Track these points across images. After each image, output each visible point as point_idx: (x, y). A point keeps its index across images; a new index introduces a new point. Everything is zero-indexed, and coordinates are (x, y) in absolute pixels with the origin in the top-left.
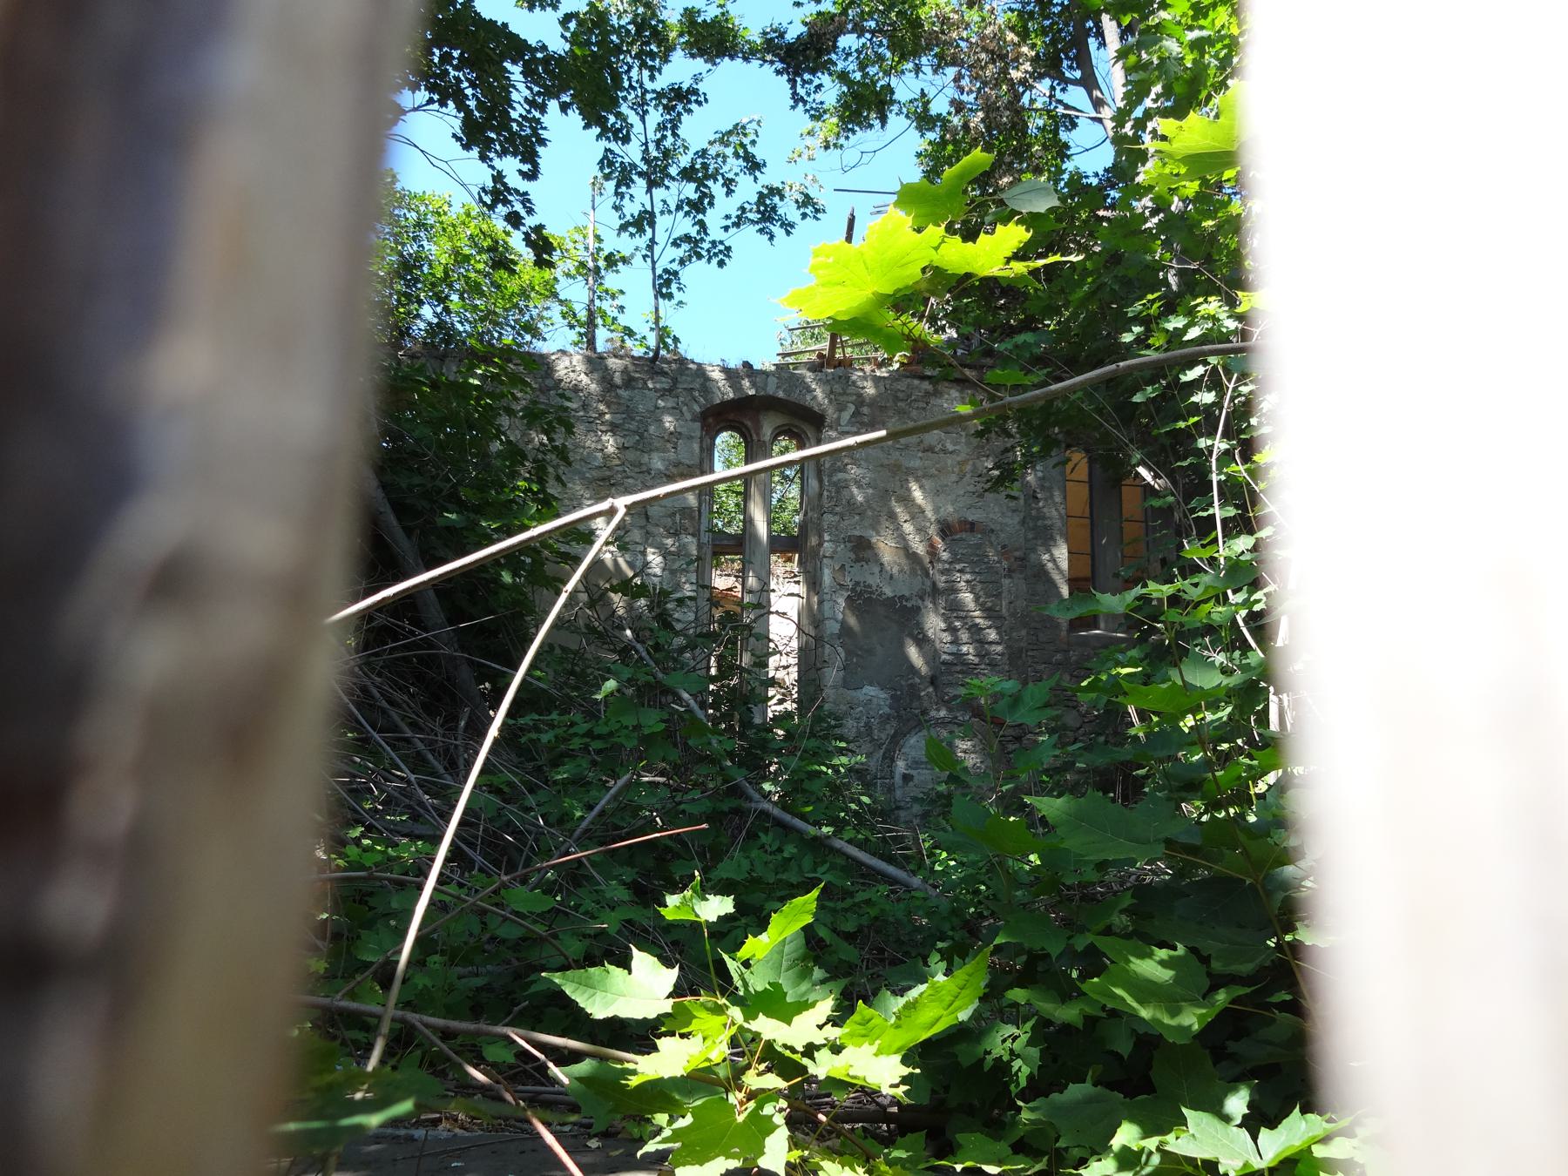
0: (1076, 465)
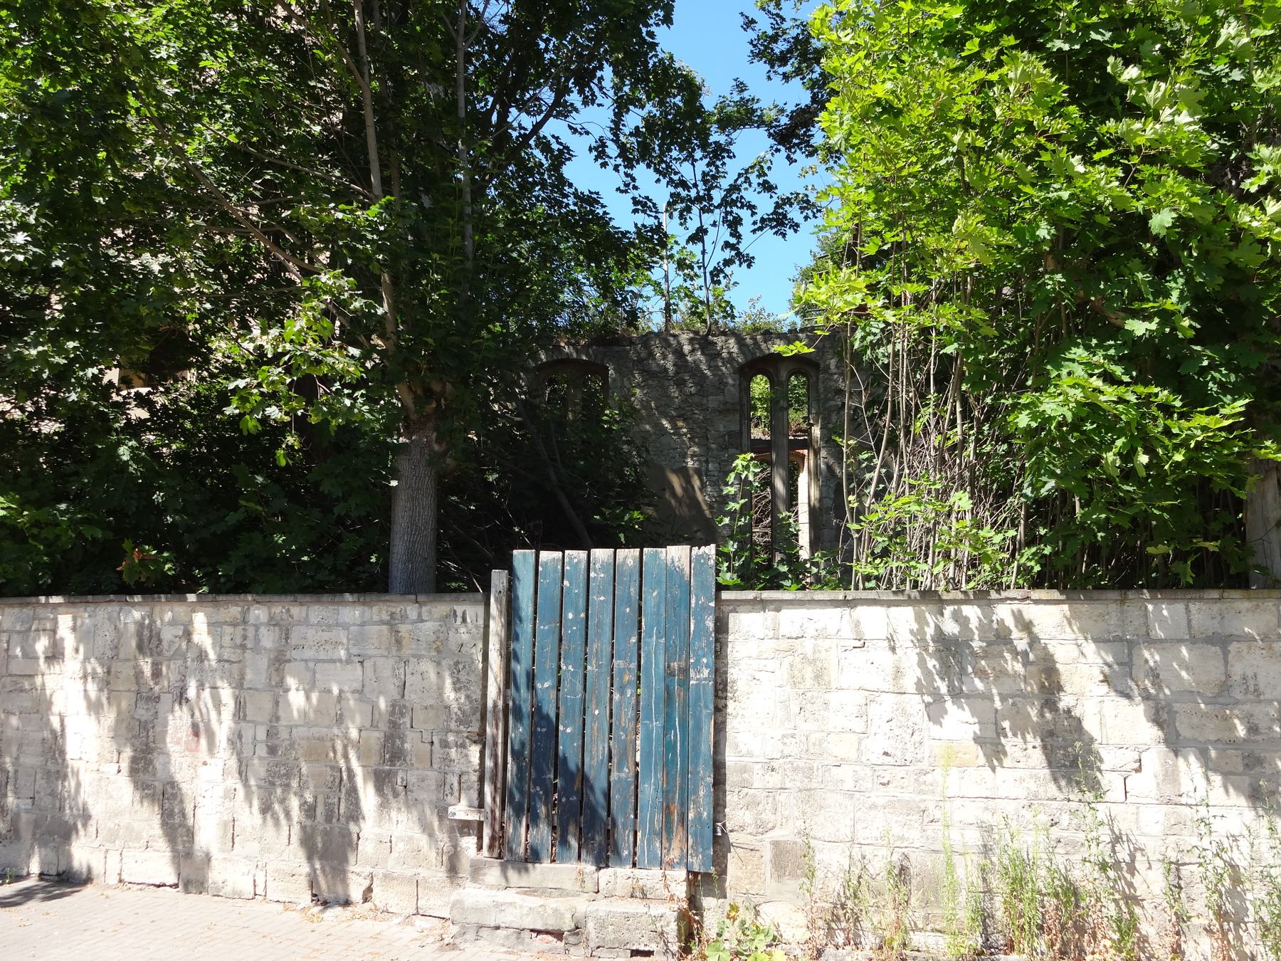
0: (612, 685)
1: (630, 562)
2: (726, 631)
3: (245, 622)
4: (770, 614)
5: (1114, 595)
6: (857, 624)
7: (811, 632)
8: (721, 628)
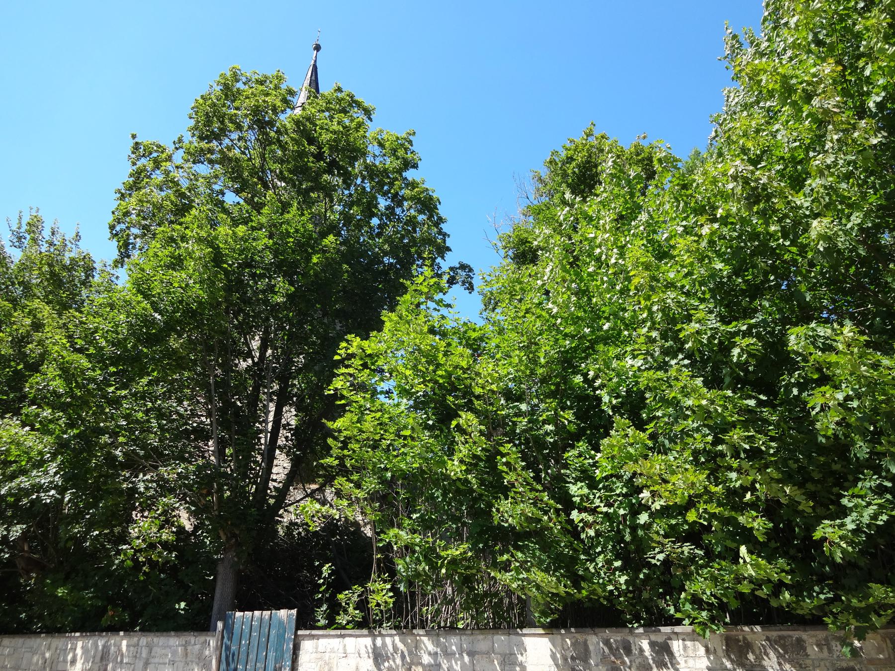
1: (267, 617)
2: (299, 649)
3: (138, 645)
4: (315, 641)
5: (506, 631)
6: (345, 646)
7: (329, 650)
8: (296, 648)
